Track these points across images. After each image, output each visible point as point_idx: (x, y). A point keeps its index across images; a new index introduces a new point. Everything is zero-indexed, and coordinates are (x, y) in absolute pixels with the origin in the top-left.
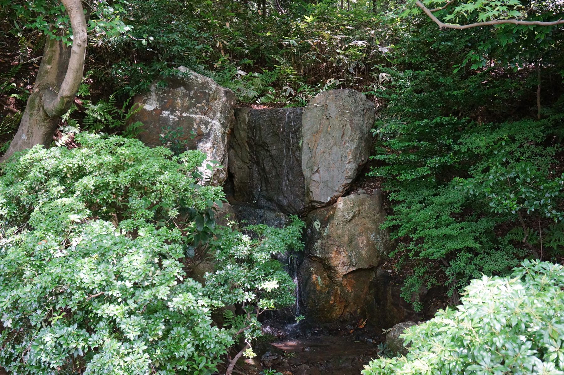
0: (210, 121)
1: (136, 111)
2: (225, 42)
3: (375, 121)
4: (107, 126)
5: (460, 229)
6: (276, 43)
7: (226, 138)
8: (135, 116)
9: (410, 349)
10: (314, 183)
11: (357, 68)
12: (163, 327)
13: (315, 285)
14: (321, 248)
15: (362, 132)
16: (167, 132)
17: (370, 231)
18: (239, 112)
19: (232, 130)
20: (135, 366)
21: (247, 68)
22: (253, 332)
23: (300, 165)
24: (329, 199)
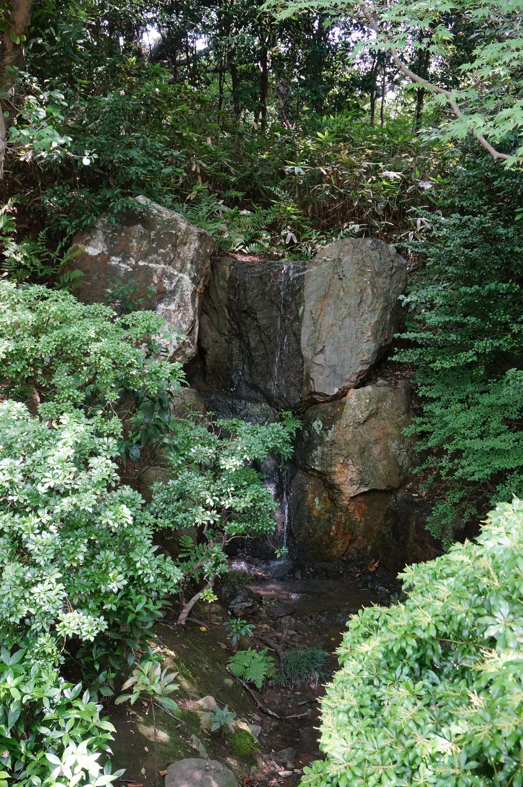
0: (176, 273)
1: (74, 255)
2: (204, 165)
3: (407, 285)
4: (34, 274)
5: (514, 442)
6: (276, 169)
7: (197, 299)
8: (72, 263)
9: (410, 594)
10: (316, 368)
11: (387, 208)
12: (85, 550)
13: (311, 509)
14: (322, 459)
15: (387, 300)
16: (116, 286)
17: (392, 438)
18: (216, 263)
19: (207, 288)
20: (45, 600)
21: (231, 203)
22: (216, 566)
23: (298, 341)
24: (336, 390)
